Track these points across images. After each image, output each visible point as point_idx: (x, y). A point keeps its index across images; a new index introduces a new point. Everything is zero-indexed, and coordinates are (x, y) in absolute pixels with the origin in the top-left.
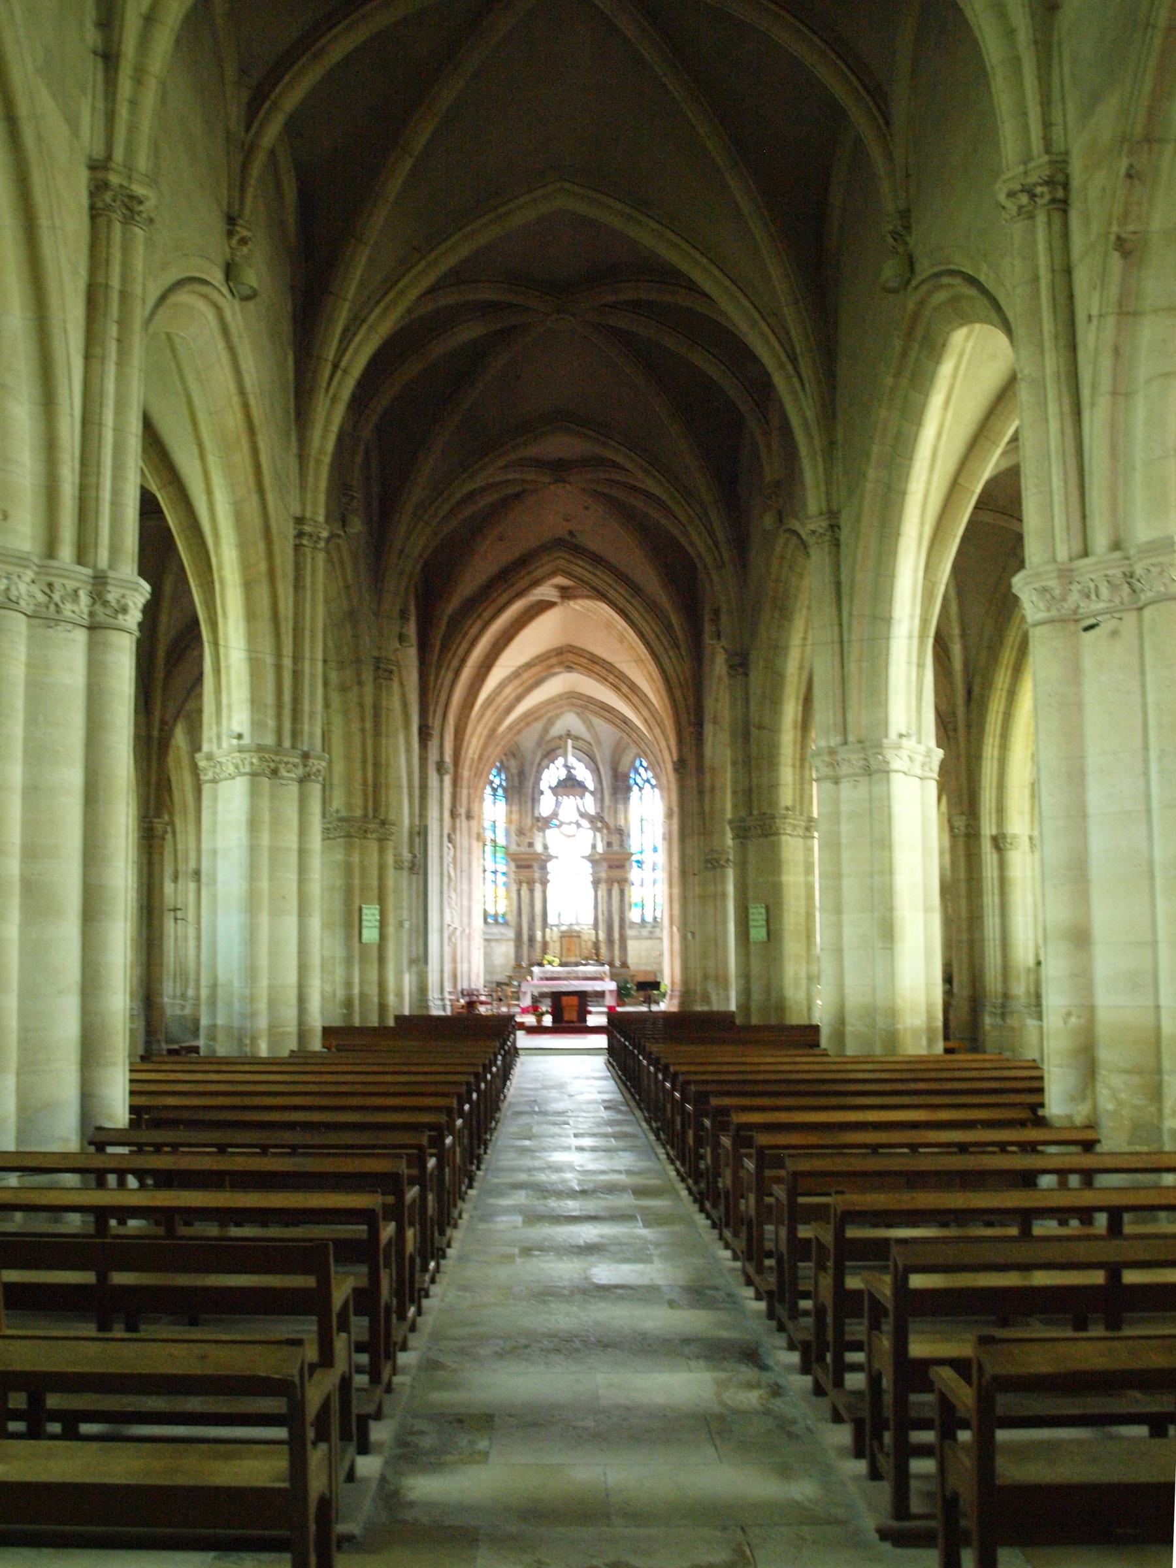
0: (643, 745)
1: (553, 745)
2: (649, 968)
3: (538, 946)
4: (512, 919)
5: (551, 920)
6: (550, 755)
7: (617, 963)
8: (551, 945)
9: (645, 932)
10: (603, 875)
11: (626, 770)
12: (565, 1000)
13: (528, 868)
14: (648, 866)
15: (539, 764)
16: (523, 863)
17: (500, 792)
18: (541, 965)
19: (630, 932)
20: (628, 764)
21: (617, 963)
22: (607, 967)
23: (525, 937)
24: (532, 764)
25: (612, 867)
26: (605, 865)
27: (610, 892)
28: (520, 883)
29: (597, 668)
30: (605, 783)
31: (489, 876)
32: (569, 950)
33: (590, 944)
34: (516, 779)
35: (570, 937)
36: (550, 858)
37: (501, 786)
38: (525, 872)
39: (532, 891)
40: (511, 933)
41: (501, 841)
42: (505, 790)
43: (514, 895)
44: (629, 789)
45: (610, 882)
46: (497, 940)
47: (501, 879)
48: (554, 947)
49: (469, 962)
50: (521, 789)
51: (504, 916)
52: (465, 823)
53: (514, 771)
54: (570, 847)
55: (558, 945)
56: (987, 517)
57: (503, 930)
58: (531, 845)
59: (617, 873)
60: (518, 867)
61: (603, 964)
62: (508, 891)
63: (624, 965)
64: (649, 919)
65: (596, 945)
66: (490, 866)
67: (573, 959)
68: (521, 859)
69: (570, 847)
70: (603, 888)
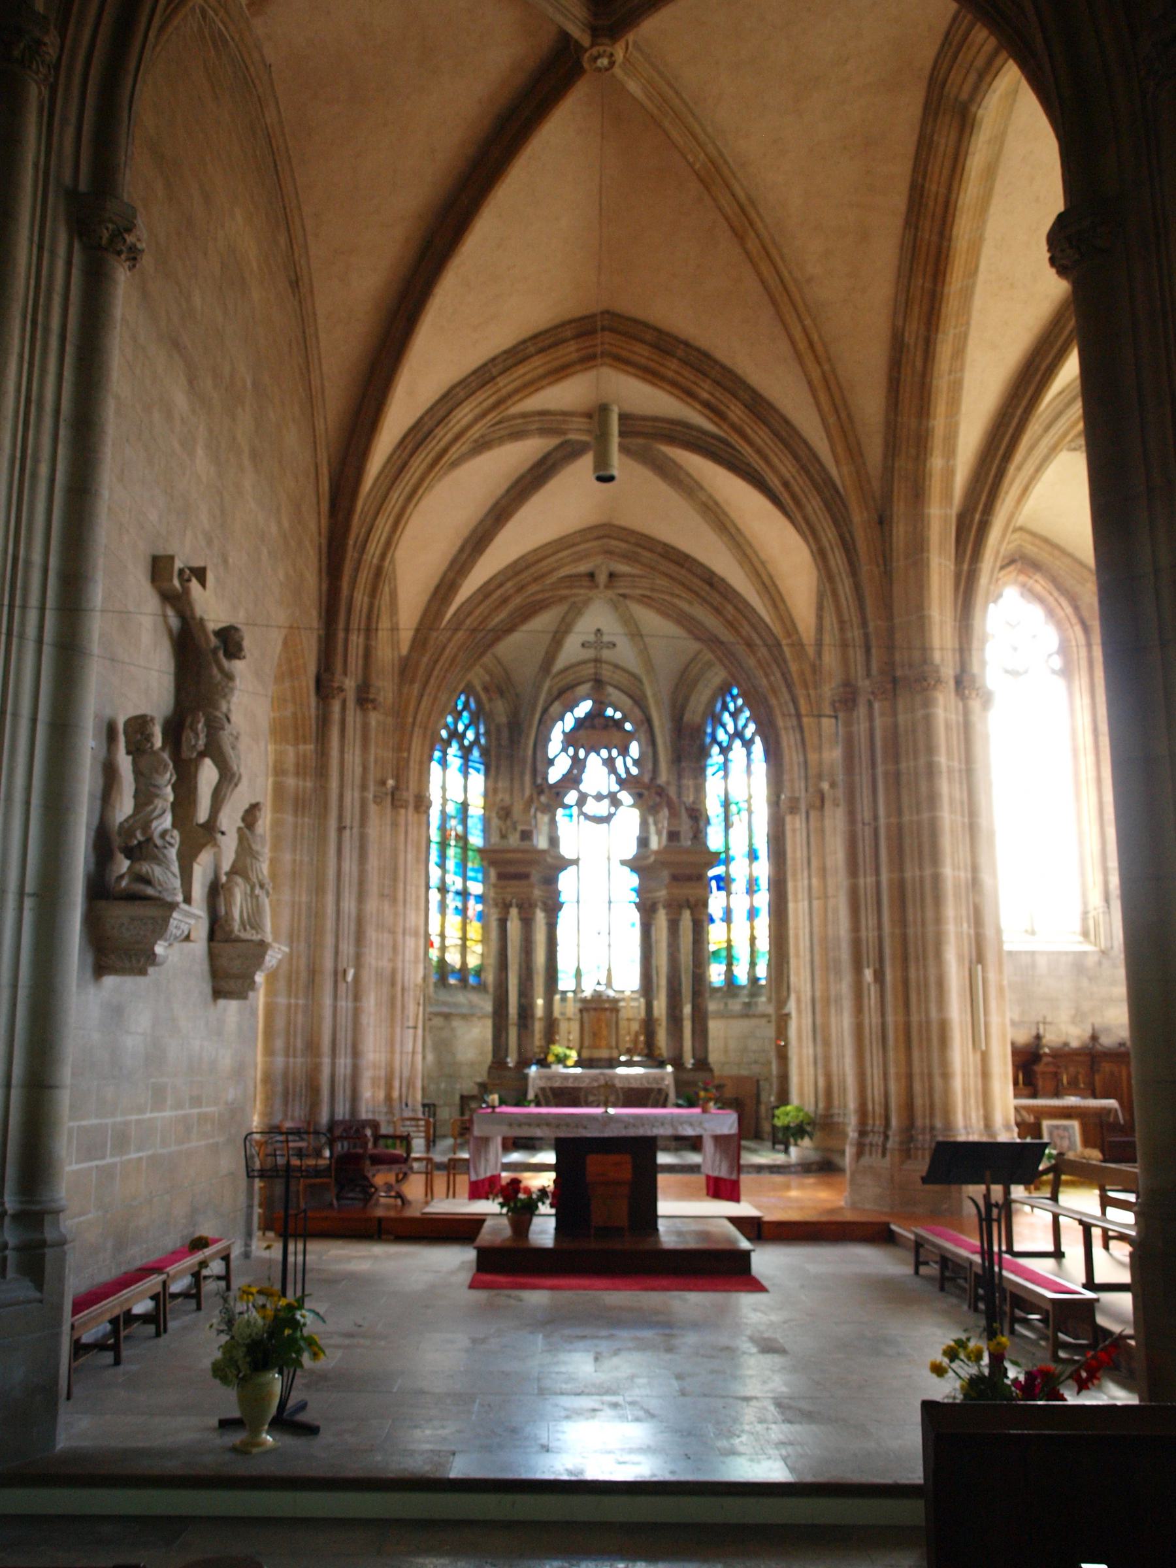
0: (746, 629)
1: (570, 678)
2: (744, 1072)
3: (538, 1027)
4: (490, 977)
5: (565, 982)
6: (565, 697)
7: (689, 1062)
8: (563, 1027)
9: (736, 1005)
10: (662, 894)
11: (698, 719)
12: (595, 1164)
13: (522, 881)
14: (739, 886)
15: (545, 711)
16: (512, 869)
17: (476, 753)
18: (543, 1063)
19: (712, 1006)
20: (701, 709)
21: (689, 1062)
22: (669, 1069)
23: (513, 1010)
24: (534, 707)
25: (676, 881)
26: (665, 874)
27: (674, 926)
28: (505, 907)
29: (671, 367)
30: (660, 741)
31: (453, 902)
32: (595, 1035)
33: (635, 1026)
34: (505, 734)
35: (600, 1010)
36: (564, 864)
37: (476, 741)
38: (514, 887)
39: (527, 923)
40: (486, 1005)
41: (476, 839)
42: (485, 752)
43: (494, 934)
44: (703, 754)
45: (675, 908)
46: (464, 1017)
47: (474, 907)
48: (569, 1030)
49: (356, 1053)
50: (510, 753)
51: (479, 971)
52: (353, 717)
53: (503, 719)
54: (598, 848)
55: (575, 1026)
56: (543, 1102)
57: (475, 998)
58: (526, 835)
59: (689, 891)
60: (501, 876)
61: (661, 1064)
62: (485, 929)
63: (702, 1064)
64: (742, 978)
65: (649, 1024)
66: (455, 882)
67: (604, 1053)
68: (510, 862)
69: (598, 848)
70: (662, 919)
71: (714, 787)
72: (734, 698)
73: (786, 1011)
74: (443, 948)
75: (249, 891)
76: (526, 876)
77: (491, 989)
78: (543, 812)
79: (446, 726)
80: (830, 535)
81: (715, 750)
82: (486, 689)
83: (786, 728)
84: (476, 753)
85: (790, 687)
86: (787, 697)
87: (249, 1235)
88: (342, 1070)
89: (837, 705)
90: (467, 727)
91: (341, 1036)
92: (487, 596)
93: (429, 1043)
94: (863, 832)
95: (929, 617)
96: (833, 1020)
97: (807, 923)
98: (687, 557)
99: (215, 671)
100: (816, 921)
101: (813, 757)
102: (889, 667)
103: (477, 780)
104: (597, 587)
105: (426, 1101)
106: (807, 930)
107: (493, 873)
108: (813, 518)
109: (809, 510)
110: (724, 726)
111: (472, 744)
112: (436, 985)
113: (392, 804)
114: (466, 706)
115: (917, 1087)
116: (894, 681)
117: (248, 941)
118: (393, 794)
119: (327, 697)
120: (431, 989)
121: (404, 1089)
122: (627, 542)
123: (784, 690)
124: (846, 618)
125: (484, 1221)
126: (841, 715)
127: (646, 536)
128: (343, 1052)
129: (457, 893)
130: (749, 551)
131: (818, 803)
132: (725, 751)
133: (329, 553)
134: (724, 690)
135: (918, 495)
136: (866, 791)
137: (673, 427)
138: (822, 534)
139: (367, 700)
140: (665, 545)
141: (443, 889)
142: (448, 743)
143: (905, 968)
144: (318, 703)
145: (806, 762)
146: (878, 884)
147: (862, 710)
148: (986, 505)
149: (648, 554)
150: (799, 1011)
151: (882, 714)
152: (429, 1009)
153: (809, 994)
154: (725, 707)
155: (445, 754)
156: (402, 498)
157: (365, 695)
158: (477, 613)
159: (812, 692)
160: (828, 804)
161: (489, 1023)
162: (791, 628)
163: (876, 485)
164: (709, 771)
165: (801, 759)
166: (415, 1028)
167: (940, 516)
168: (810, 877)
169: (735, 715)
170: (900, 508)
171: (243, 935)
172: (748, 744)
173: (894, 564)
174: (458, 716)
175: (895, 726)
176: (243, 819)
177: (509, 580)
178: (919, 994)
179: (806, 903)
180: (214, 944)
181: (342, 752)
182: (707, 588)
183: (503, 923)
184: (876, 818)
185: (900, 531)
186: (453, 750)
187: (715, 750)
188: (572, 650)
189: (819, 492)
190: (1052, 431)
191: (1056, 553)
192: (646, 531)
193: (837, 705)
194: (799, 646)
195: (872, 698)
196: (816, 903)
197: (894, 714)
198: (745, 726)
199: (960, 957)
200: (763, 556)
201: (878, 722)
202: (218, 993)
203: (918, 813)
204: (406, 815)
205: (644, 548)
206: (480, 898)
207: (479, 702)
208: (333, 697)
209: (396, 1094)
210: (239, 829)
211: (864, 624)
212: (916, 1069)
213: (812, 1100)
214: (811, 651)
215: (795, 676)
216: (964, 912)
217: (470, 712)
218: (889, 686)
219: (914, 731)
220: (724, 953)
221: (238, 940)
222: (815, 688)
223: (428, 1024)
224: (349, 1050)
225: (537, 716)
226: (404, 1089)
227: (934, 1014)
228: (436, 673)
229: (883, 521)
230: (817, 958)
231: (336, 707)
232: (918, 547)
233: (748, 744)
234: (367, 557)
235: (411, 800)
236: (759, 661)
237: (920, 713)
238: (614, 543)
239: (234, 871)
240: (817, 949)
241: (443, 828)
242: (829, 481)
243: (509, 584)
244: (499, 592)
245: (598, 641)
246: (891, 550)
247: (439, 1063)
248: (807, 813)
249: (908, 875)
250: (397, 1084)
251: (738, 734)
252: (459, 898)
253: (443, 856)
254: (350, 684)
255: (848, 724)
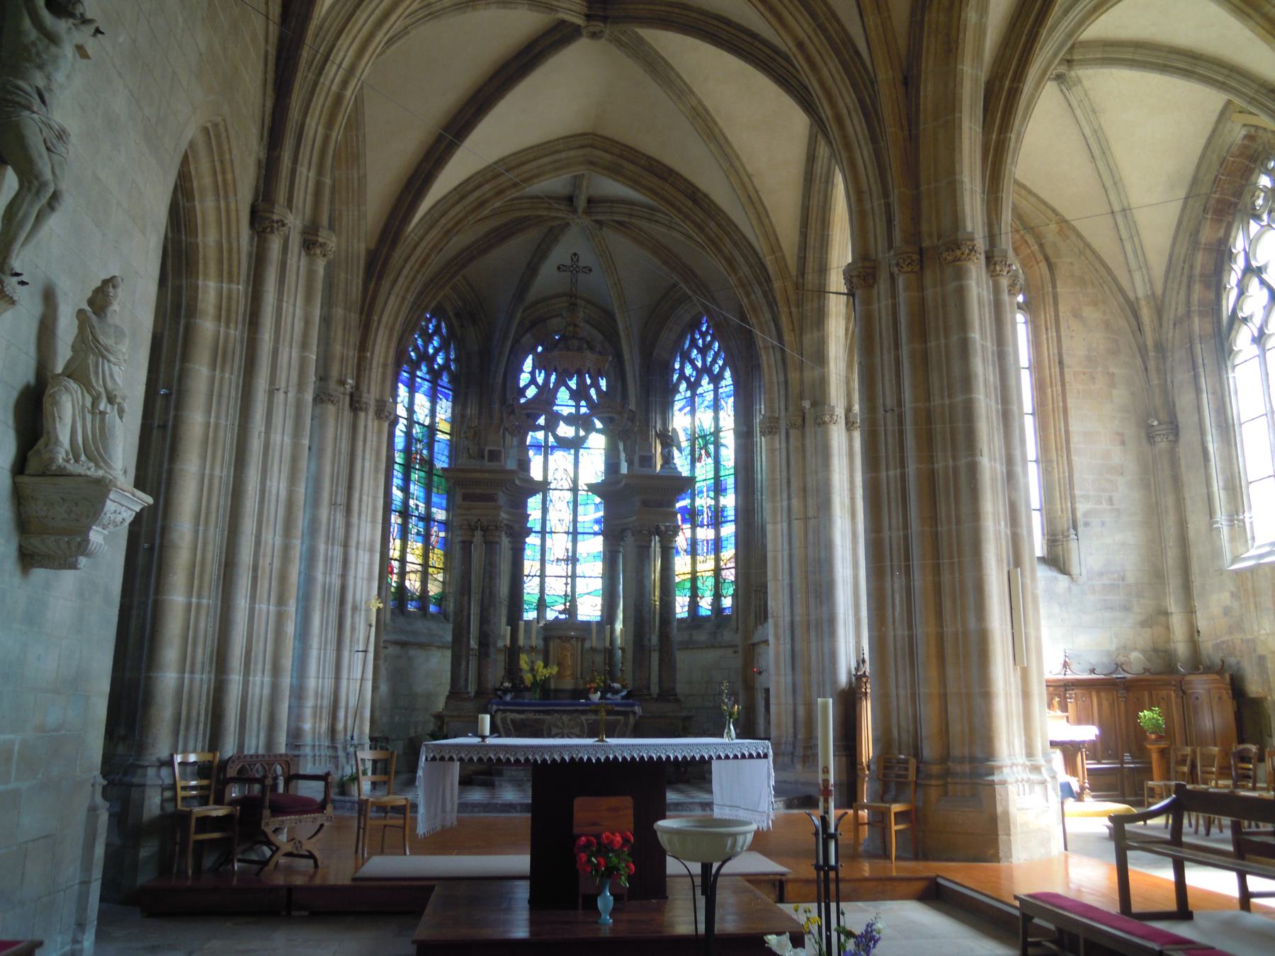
9: (701, 636)
15: (517, 341)
17: (445, 378)
25: (640, 510)
30: (629, 375)
31: (415, 526)
37: (445, 367)
39: (491, 546)
41: (441, 462)
42: (454, 379)
43: (457, 562)
51: (440, 599)
54: (569, 471)
58: (494, 456)
64: (705, 605)
66: (417, 504)
71: (680, 421)
72: (703, 335)
73: (757, 638)
74: (403, 574)
75: (89, 404)
76: (491, 498)
77: (451, 619)
78: (512, 434)
79: (416, 349)
80: (848, 100)
81: (683, 386)
82: (457, 315)
83: (766, 348)
84: (445, 378)
85: (772, 304)
86: (768, 316)
87: (81, 926)
88: (257, 690)
89: (855, 280)
90: (437, 351)
91: (258, 647)
92: (462, 198)
93: (383, 672)
94: (885, 418)
95: (962, 182)
96: (813, 646)
97: (786, 546)
98: (671, 171)
99: (27, 23)
100: (796, 543)
101: (794, 376)
102: (914, 236)
103: (445, 409)
104: (575, 211)
105: (376, 735)
106: (786, 553)
107: (459, 493)
108: (830, 82)
109: (825, 72)
110: (692, 362)
111: (442, 368)
112: (393, 613)
113: (351, 405)
114: (437, 330)
115: (954, 710)
116: (921, 252)
117: (80, 475)
118: (352, 395)
119: (264, 231)
120: (388, 615)
121: (350, 721)
122: (612, 154)
123: (765, 308)
124: (865, 187)
125: (432, 888)
126: (858, 293)
127: (631, 148)
128: (260, 667)
129: (420, 518)
130: (737, 163)
131: (799, 421)
132: (693, 386)
133: (278, 58)
134: (695, 325)
135: (951, 49)
136: (889, 375)
137: (670, 9)
138: (839, 99)
139: (315, 243)
140: (649, 158)
141: (405, 513)
142: (415, 366)
143: (937, 569)
144: (252, 238)
145: (786, 382)
146: (903, 477)
147: (883, 285)
148: (1015, 73)
149: (632, 167)
150: (777, 637)
151: (906, 289)
152: (384, 637)
153: (787, 619)
154: (694, 343)
155: (413, 376)
156: (370, 22)
157: (313, 238)
158: (452, 213)
159: (794, 310)
160: (809, 421)
161: (449, 653)
162: (775, 247)
163: (902, 42)
164: (677, 406)
165: (782, 378)
166: (366, 651)
167: (972, 75)
168: (789, 498)
169: (703, 352)
170: (929, 64)
171: (71, 467)
172: (716, 380)
173: (921, 127)
174: (428, 339)
175: (922, 301)
176: (91, 302)
177: (487, 182)
178: (954, 600)
179: (785, 525)
180: (23, 479)
181: (280, 300)
182: (690, 204)
183: (467, 545)
184: (900, 403)
185: (929, 91)
186: (422, 372)
187: (683, 386)
188: (548, 276)
189: (838, 53)
190: (1071, 15)
191: (1023, 192)
192: (630, 144)
193: (855, 280)
194: (781, 260)
195: (896, 270)
196: (796, 523)
197: (921, 288)
198: (714, 361)
199: (999, 560)
200: (750, 170)
201: (902, 296)
202: (28, 559)
203: (950, 396)
204: (366, 419)
205: (628, 160)
206: (445, 525)
207: (449, 327)
208: (272, 232)
209: (340, 726)
210: (81, 312)
211: (886, 194)
212: (952, 688)
213: (791, 730)
214: (793, 269)
215: (778, 296)
216: (1001, 510)
217: (442, 337)
218: (915, 257)
219: (945, 306)
220: (688, 585)
221: (62, 474)
222: (798, 306)
223: (383, 653)
224: (268, 666)
225: (509, 343)
226: (350, 721)
227: (972, 624)
228: (405, 272)
229: (909, 82)
230: (798, 581)
231: (275, 245)
232: (950, 106)
233: (716, 380)
234: (325, 81)
235: (372, 403)
236: (740, 280)
237: (951, 286)
238: (598, 153)
239: (70, 372)
240: (797, 571)
241: (407, 451)
242: (849, 42)
243: (487, 187)
244: (476, 194)
245: (573, 268)
246: (918, 110)
247: (394, 693)
248: (787, 433)
249: (939, 466)
250: (341, 714)
251: (707, 370)
252: (421, 524)
253: (407, 479)
254: (294, 222)
255: (867, 302)
